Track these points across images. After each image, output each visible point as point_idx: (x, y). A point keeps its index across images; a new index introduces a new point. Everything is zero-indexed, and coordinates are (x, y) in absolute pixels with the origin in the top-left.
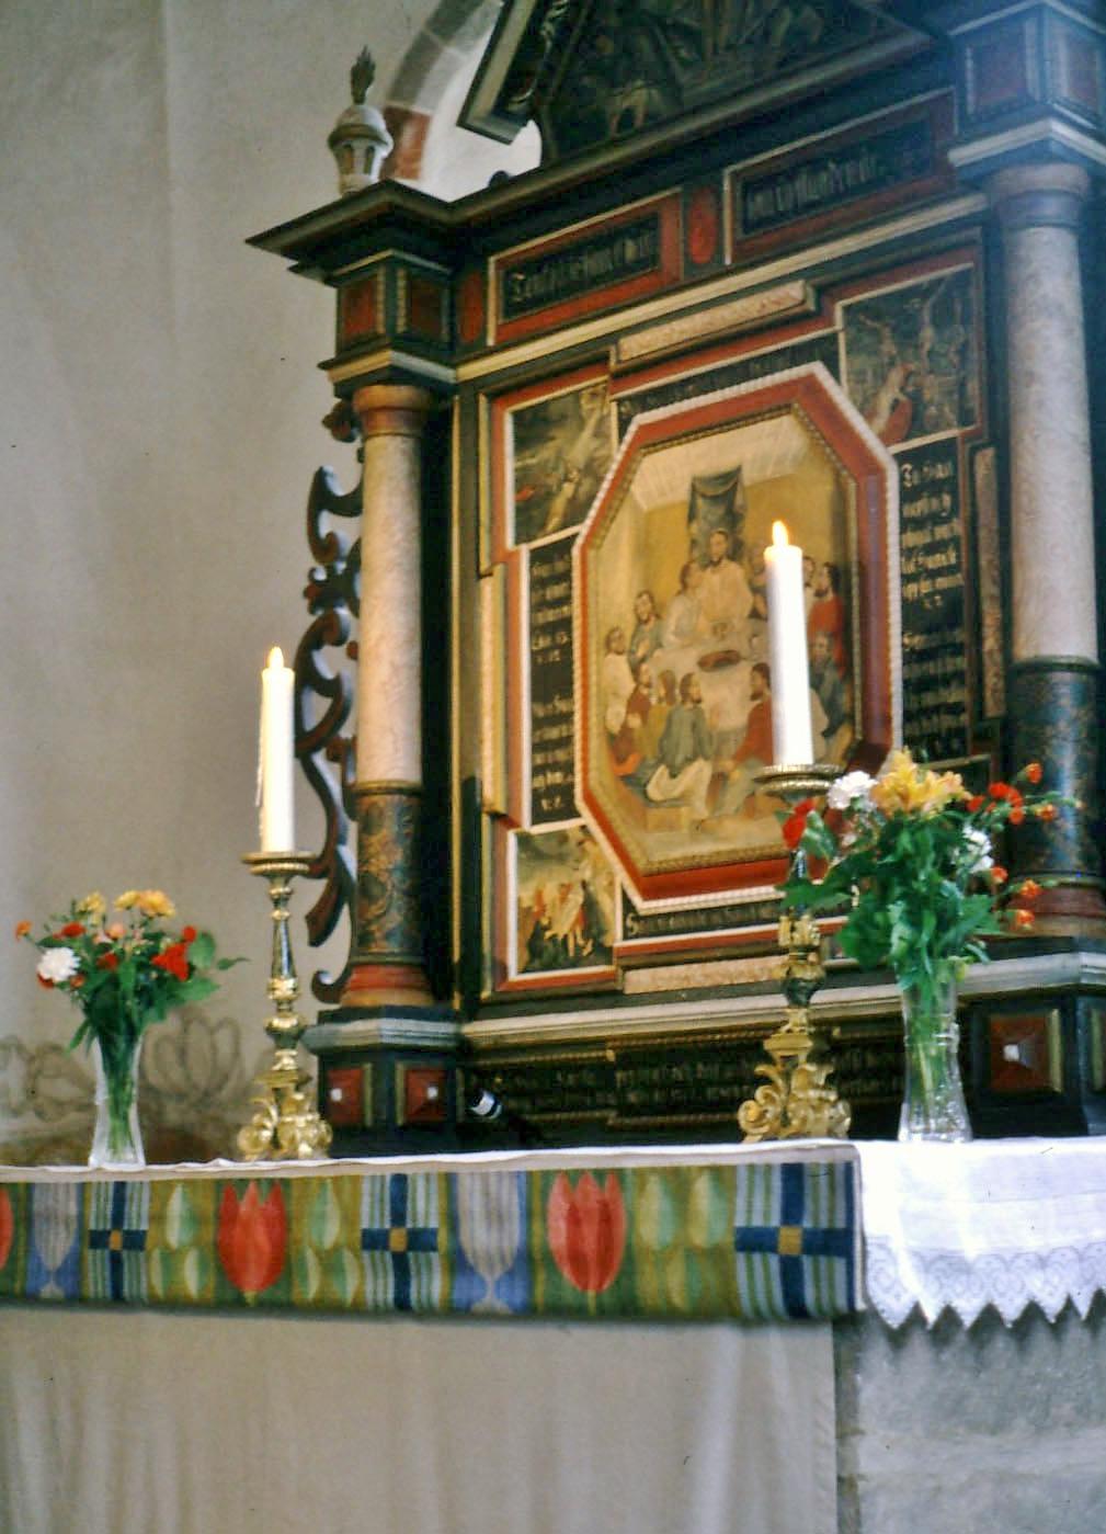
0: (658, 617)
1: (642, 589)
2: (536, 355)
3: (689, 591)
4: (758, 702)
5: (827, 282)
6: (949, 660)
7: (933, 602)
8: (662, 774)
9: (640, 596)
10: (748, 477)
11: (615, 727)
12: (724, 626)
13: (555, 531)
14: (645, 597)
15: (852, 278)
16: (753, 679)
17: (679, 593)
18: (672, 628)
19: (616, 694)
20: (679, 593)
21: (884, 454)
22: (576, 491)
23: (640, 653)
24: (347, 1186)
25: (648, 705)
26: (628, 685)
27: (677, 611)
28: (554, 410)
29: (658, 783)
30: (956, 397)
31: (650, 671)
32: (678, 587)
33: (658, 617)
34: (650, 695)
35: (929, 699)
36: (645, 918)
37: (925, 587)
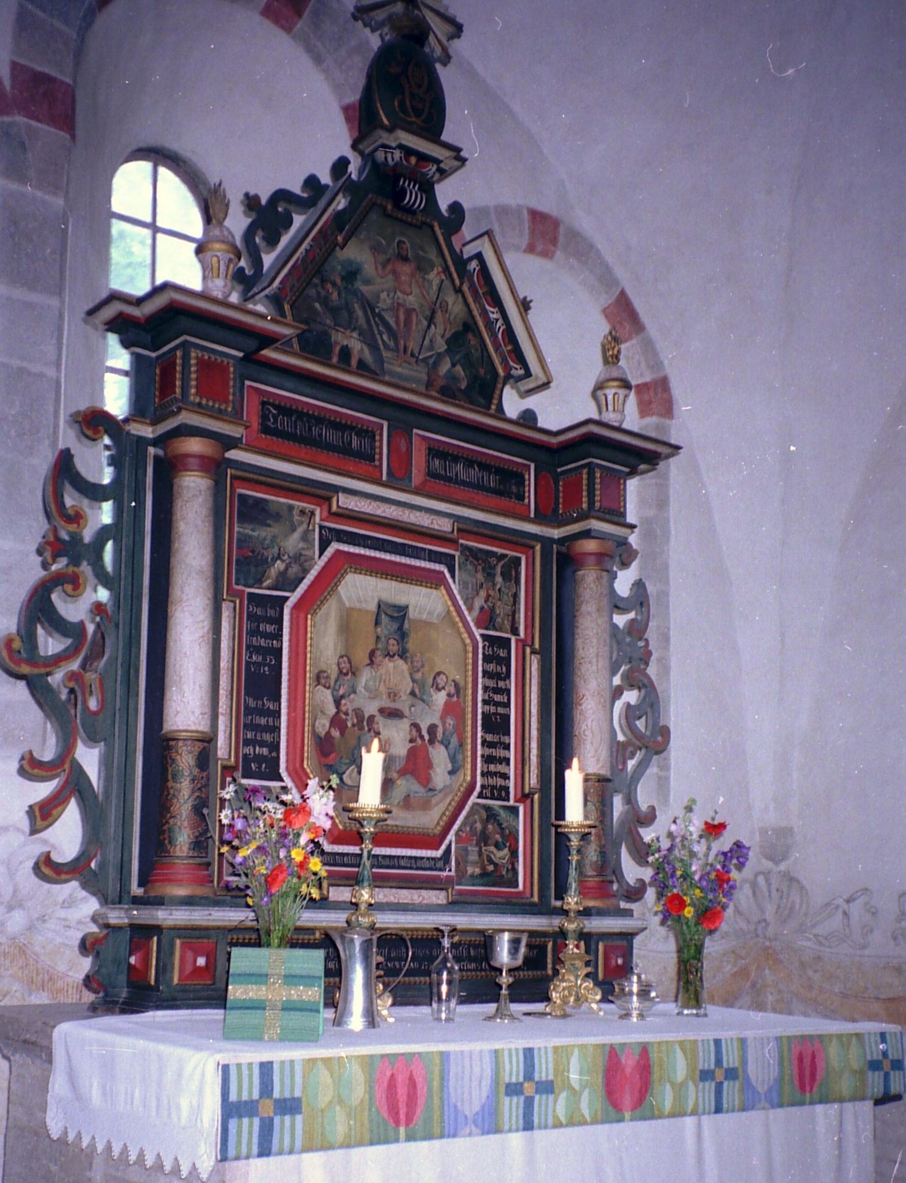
0: (354, 674)
2: (245, 461)
4: (414, 744)
5: (468, 528)
7: (496, 719)
8: (353, 770)
9: (342, 657)
10: (412, 614)
11: (322, 732)
12: (395, 695)
13: (269, 588)
16: (411, 730)
17: (368, 665)
18: (363, 684)
20: (368, 665)
21: (477, 633)
22: (286, 569)
23: (341, 692)
24: (706, 1042)
26: (332, 710)
27: (366, 676)
29: (351, 774)
30: (510, 618)
33: (354, 674)
34: (347, 720)
35: (492, 768)
36: (329, 854)
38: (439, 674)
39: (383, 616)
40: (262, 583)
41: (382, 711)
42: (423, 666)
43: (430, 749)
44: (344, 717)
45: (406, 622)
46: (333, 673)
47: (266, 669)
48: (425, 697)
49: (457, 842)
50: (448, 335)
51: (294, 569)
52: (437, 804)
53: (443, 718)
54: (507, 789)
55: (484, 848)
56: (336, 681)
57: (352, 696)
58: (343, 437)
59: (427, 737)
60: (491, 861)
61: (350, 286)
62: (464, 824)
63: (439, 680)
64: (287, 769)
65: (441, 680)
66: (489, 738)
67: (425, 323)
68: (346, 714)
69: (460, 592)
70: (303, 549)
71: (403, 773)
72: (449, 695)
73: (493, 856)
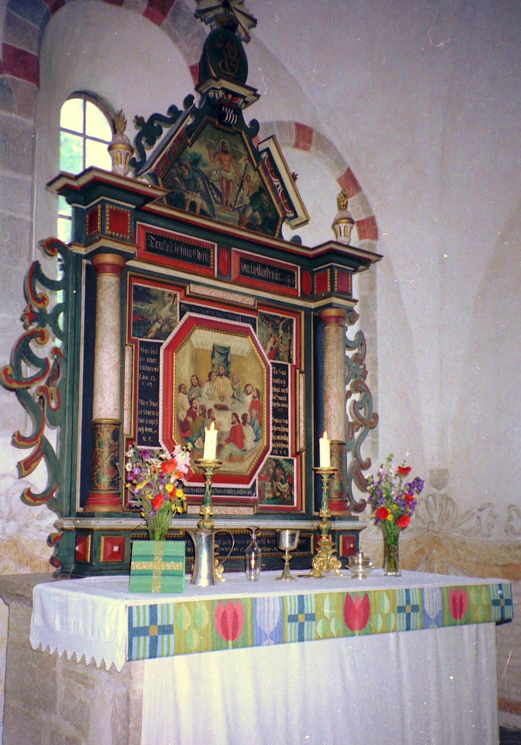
0: (200, 386)
1: (194, 374)
3: (212, 381)
4: (234, 425)
5: (263, 303)
6: (284, 428)
7: (280, 410)
8: (200, 440)
9: (193, 376)
10: (232, 351)
12: (223, 397)
14: (195, 377)
15: (268, 306)
16: (232, 417)
17: (208, 381)
18: (205, 391)
19: (183, 408)
20: (208, 381)
21: (269, 362)
22: (161, 327)
23: (193, 396)
25: (196, 415)
26: (188, 406)
27: (207, 387)
28: (153, 293)
29: (199, 442)
31: (196, 403)
32: (208, 379)
33: (200, 386)
34: (196, 412)
35: (278, 438)
36: (187, 487)
37: (278, 405)
38: (248, 385)
39: (216, 353)
40: (148, 335)
41: (216, 406)
42: (239, 381)
43: (244, 428)
44: (194, 410)
45: (229, 356)
46: (188, 385)
47: (151, 383)
48: (240, 398)
49: (259, 480)
50: (250, 195)
51: (166, 327)
52: (247, 459)
53: (250, 410)
54: (287, 449)
55: (274, 483)
56: (190, 390)
57: (199, 398)
58: (192, 252)
59: (241, 421)
60: (278, 490)
61: (195, 168)
62: (263, 470)
63: (248, 389)
64: (163, 440)
65: (249, 389)
66: (277, 421)
67: (238, 188)
68: (196, 408)
69: (259, 339)
70: (171, 316)
71: (228, 441)
72: (254, 397)
73: (279, 488)
